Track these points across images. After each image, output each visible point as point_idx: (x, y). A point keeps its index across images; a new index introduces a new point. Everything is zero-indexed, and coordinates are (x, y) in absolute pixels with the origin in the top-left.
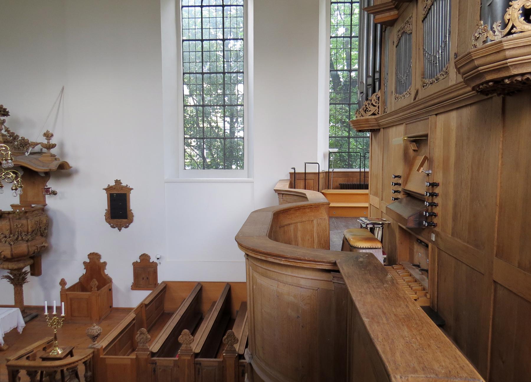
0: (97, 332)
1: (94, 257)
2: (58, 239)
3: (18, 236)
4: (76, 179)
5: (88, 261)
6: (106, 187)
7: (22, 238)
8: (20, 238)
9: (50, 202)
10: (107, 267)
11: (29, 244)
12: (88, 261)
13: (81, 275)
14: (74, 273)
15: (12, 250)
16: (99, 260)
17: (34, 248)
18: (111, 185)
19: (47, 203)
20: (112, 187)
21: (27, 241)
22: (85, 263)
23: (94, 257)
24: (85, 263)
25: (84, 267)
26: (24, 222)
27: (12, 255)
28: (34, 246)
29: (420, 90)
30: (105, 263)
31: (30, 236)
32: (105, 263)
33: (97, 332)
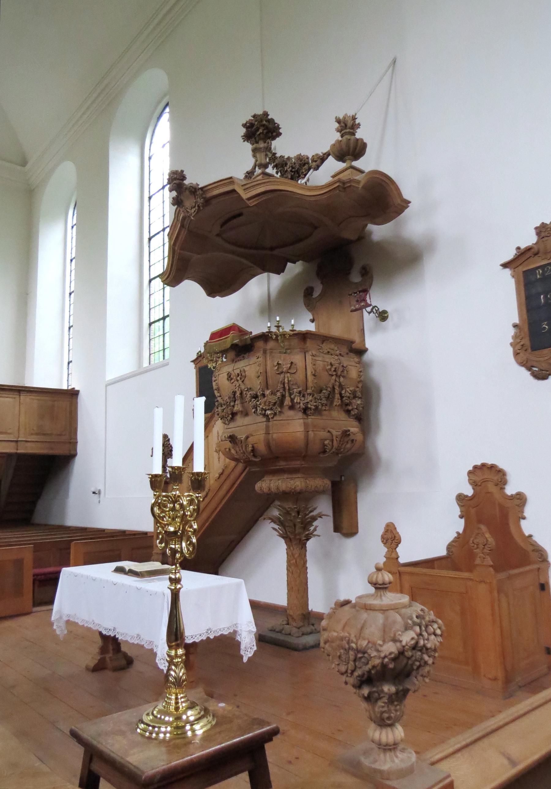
0: (388, 634)
1: (488, 477)
2: (395, 437)
3: (283, 396)
4: (431, 267)
5: (469, 491)
6: (510, 255)
7: (292, 400)
8: (287, 402)
9: (378, 344)
10: (528, 511)
11: (310, 420)
12: (469, 491)
13: (451, 536)
14: (430, 528)
15: (267, 433)
16: (503, 489)
17: (323, 434)
18: (523, 246)
19: (367, 346)
20: (529, 249)
21: (305, 411)
22: (461, 498)
23: (488, 477)
24: (461, 498)
25: (457, 511)
26: (298, 358)
27: (268, 445)
28: (324, 429)
29: (429, 762)
30: (520, 499)
31: (310, 398)
32: (520, 499)
33: (388, 634)
